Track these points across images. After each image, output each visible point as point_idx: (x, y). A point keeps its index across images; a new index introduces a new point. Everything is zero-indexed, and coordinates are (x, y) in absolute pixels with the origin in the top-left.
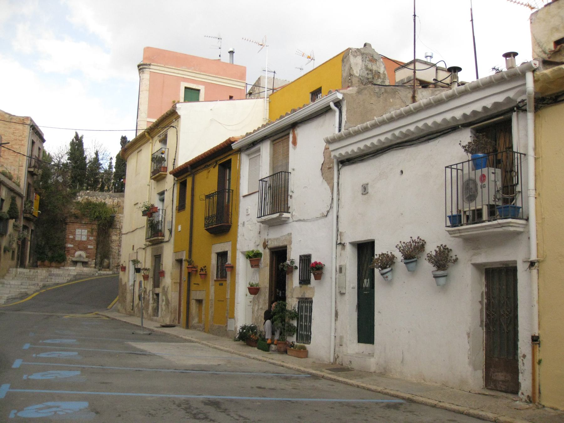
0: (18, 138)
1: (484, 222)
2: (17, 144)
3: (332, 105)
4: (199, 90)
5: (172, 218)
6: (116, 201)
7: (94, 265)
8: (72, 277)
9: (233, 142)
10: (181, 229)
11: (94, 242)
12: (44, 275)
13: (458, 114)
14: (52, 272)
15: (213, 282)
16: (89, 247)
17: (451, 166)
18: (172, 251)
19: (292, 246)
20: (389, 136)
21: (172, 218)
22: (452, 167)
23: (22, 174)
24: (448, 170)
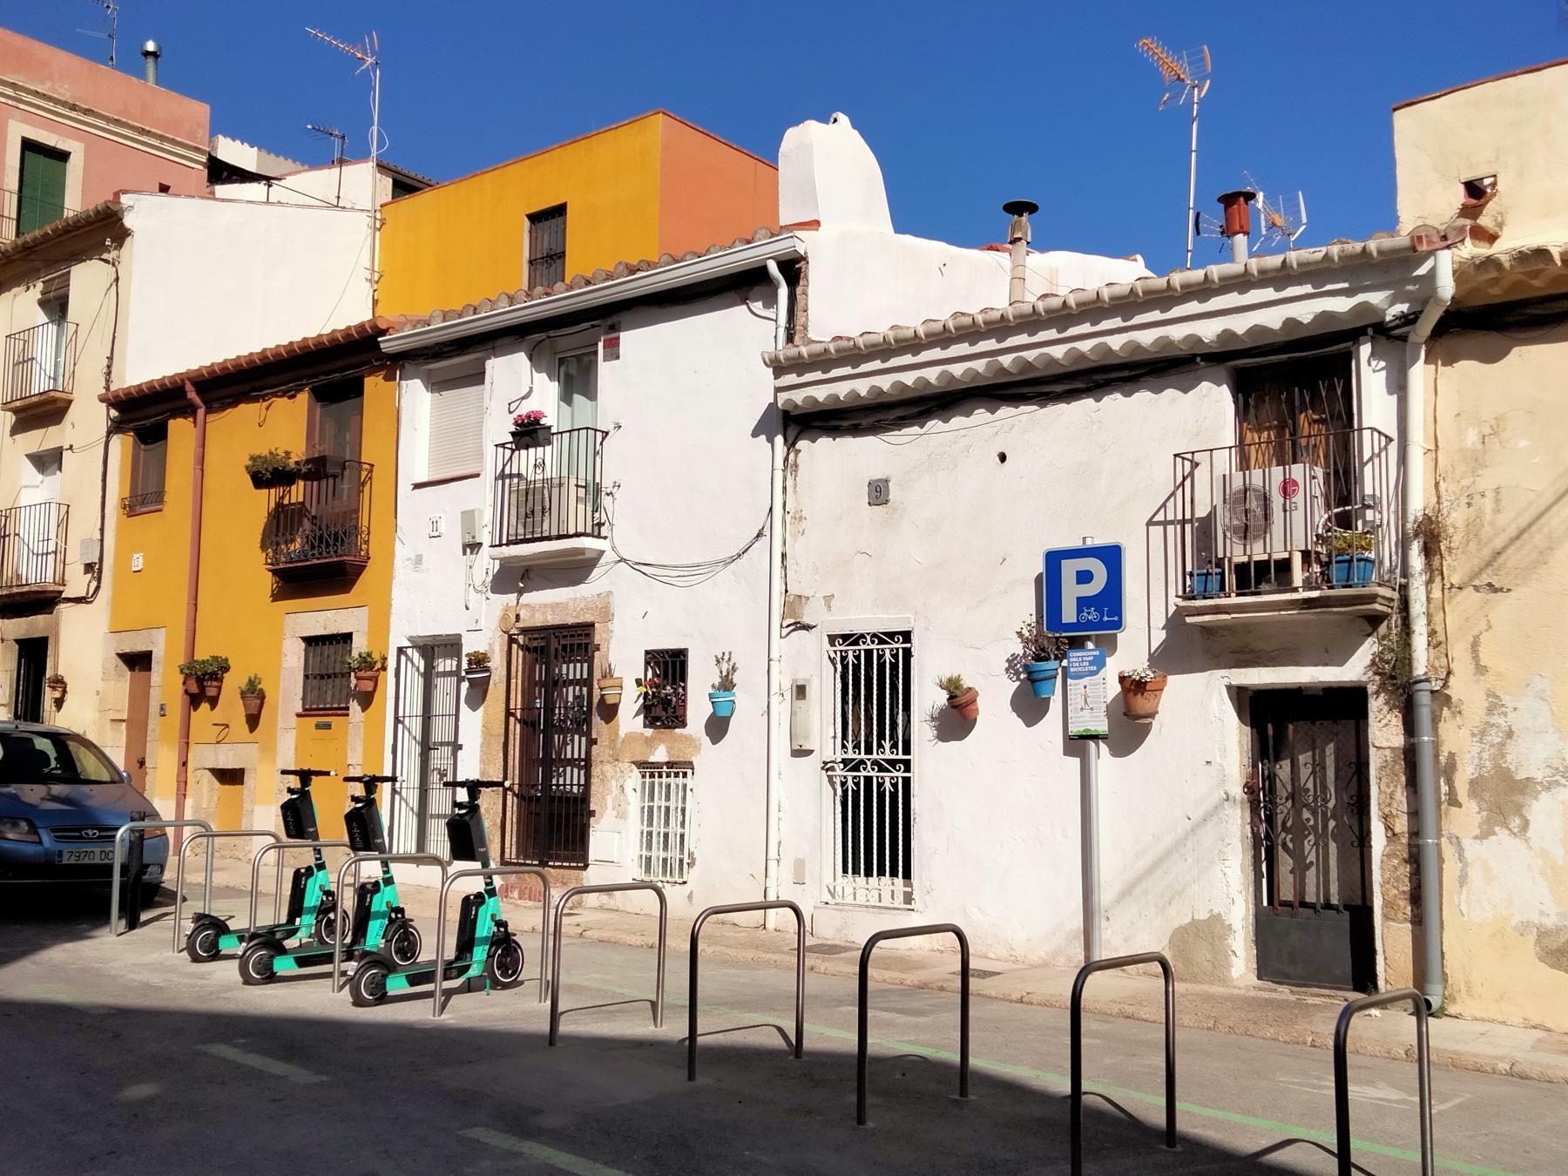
1: (1295, 590)
3: (773, 267)
4: (63, 156)
5: (102, 530)
9: (383, 332)
10: (143, 564)
13: (1209, 331)
15: (294, 721)
17: (504, 444)
18: (105, 628)
19: (615, 625)
20: (980, 365)
21: (102, 530)
22: (506, 446)
24: (500, 450)
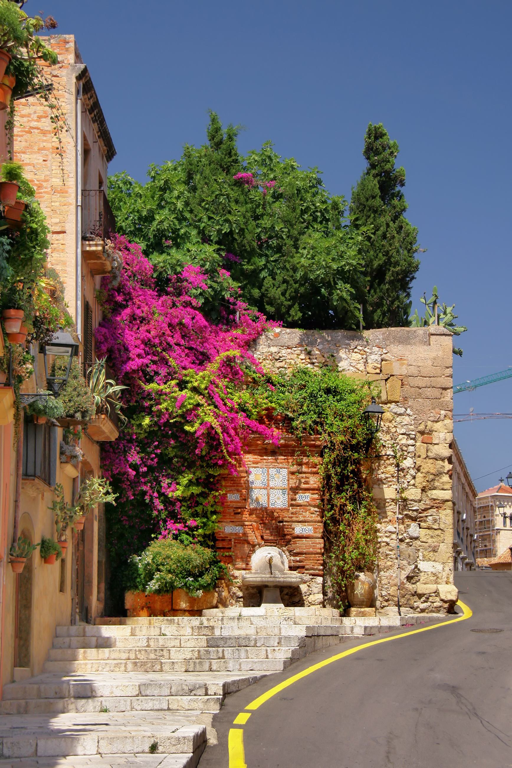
0: (34, 124)
2: (36, 148)
6: (374, 358)
7: (320, 597)
8: (295, 645)
11: (313, 514)
12: (192, 643)
14: (217, 633)
16: (299, 529)
23: (64, 263)
